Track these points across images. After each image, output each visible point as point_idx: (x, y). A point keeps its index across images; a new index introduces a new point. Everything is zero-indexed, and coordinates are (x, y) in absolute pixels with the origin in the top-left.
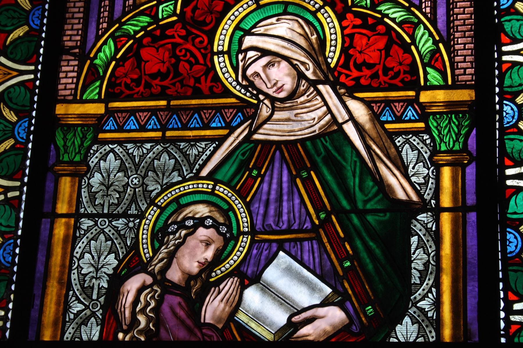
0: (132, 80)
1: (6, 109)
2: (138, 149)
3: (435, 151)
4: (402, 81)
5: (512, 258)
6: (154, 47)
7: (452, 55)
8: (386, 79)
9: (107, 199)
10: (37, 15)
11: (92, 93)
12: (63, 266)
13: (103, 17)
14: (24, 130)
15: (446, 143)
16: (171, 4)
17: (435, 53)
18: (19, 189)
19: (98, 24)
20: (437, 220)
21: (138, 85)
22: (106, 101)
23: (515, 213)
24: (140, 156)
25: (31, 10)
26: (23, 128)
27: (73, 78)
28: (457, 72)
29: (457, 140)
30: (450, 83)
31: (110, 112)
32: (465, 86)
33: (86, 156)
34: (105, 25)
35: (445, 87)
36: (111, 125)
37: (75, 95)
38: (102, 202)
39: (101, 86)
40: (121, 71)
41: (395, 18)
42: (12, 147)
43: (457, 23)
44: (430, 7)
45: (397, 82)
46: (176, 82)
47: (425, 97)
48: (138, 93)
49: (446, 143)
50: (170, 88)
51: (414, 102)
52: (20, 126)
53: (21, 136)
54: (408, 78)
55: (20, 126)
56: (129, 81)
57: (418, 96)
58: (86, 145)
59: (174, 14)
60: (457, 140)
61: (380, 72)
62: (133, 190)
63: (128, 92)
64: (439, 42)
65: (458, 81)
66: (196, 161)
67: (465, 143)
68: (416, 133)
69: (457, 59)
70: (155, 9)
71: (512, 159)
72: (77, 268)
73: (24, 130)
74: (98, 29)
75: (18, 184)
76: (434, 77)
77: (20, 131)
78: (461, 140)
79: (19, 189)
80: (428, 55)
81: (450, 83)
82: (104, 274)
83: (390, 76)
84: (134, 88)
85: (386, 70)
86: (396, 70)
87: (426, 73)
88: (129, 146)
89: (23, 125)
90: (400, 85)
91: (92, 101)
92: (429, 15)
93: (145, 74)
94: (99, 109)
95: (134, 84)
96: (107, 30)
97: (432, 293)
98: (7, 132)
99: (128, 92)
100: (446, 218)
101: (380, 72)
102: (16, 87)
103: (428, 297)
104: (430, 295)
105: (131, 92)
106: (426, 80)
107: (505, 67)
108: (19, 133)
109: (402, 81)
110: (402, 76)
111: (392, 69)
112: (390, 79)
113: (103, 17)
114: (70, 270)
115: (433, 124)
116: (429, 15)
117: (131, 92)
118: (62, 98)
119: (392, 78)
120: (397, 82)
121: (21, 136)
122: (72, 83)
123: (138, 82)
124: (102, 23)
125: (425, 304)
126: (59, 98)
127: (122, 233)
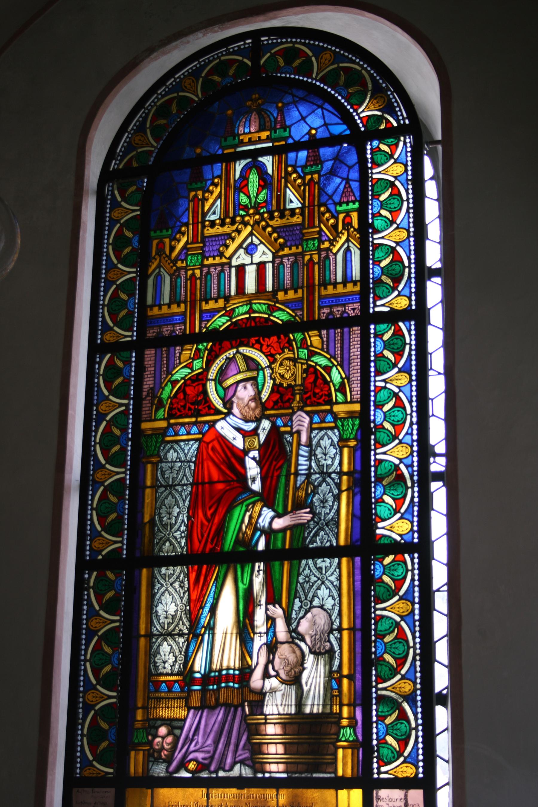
0: (181, 406)
1: (106, 645)
3: (341, 439)
5: (379, 354)
8: (315, 399)
9: (171, 475)
10: (113, 733)
11: (161, 414)
12: (146, 647)
20: (340, 478)
21: (185, 409)
22: (167, 419)
23: (380, 331)
25: (115, 580)
27: (149, 407)
28: (353, 393)
30: (349, 400)
33: (159, 451)
34: (165, 376)
35: (346, 402)
36: (171, 432)
37: (151, 417)
39: (164, 411)
42: (123, 381)
43: (353, 364)
45: (321, 401)
47: (336, 408)
51: (331, 412)
54: (327, 399)
56: (179, 407)
57: (332, 408)
58: (158, 445)
59: (202, 368)
60: (352, 433)
63: (179, 413)
67: (356, 434)
68: (332, 429)
69: (353, 386)
72: (161, 468)
74: (161, 378)
76: (340, 397)
78: (354, 433)
80: (338, 385)
86: (320, 394)
87: (336, 396)
90: (323, 403)
91: (161, 420)
99: (179, 413)
106: (336, 399)
107: (374, 181)
109: (324, 400)
110: (323, 398)
115: (339, 423)
119: (319, 399)
120: (321, 401)
123: (184, 407)
127: (178, 590)
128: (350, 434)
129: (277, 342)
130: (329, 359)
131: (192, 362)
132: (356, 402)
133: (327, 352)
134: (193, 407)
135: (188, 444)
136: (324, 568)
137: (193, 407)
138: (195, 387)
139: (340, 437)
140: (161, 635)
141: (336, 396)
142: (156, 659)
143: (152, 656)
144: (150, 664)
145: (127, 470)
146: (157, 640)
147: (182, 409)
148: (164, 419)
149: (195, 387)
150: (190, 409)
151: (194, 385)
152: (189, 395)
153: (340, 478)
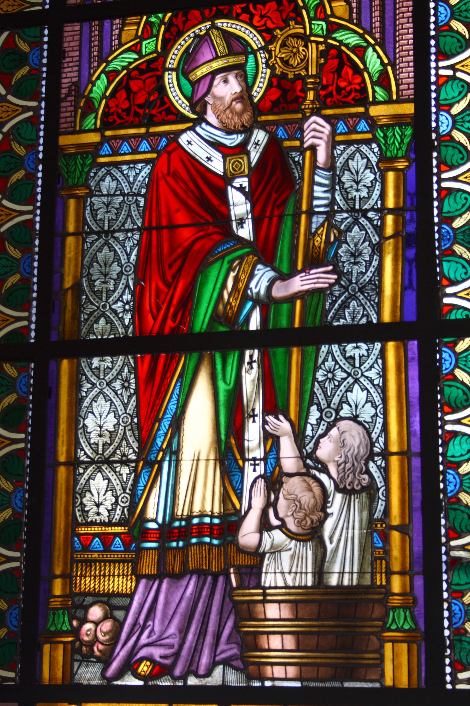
0: (123, 110)
2: (129, 240)
4: (354, 99)
6: (141, 79)
7: (398, 72)
8: (339, 97)
9: (107, 215)
11: (90, 122)
13: (94, 56)
14: (37, 57)
15: (391, 151)
16: (153, 41)
17: (384, 75)
18: (32, 212)
19: (90, 63)
20: (382, 219)
21: (128, 115)
24: (127, 474)
26: (36, 55)
29: (401, 148)
30: (395, 97)
31: (105, 139)
32: (407, 101)
33: (87, 179)
34: (96, 64)
35: (389, 101)
36: (106, 149)
38: (103, 218)
39: (96, 118)
40: (111, 104)
41: (349, 43)
44: (380, 32)
46: (162, 111)
47: (374, 111)
48: (128, 121)
49: (391, 151)
50: (157, 116)
51: (366, 116)
52: (34, 54)
53: (35, 62)
55: (34, 54)
56: (120, 111)
57: (367, 110)
61: (334, 93)
62: (122, 509)
64: (387, 64)
65: (402, 96)
66: (179, 384)
69: (402, 75)
70: (139, 46)
71: (449, 279)
73: (37, 57)
75: (30, 208)
76: (380, 94)
77: (34, 58)
79: (32, 212)
80: (377, 75)
81: (395, 97)
82: (106, 432)
83: (342, 96)
84: (125, 117)
85: (339, 90)
87: (374, 91)
88: (124, 167)
89: (36, 53)
90: (353, 102)
91: (90, 131)
92: (379, 40)
93: (134, 105)
94: (94, 138)
95: (124, 113)
96: (99, 66)
97: (377, 363)
98: (10, 387)
100: (395, 461)
101: (334, 93)
102: (24, 124)
103: (374, 367)
104: (376, 366)
105: (123, 121)
106: (374, 97)
108: (33, 60)
111: (344, 88)
112: (343, 97)
113: (94, 35)
114: (74, 507)
115: (380, 134)
116: (379, 40)
117: (123, 121)
118: (64, 130)
119: (345, 97)
121: (35, 62)
122: (71, 117)
123: (128, 111)
124: (94, 41)
125: (372, 374)
126: (61, 130)
127: (119, 392)
131: (140, 43)
134: (141, 111)
136: (357, 358)
137: (141, 111)
139: (381, 154)
140: (93, 462)
141: (374, 91)
143: (78, 496)
145: (36, 208)
146: (85, 469)
147: (124, 115)
150: (137, 114)
151: (143, 77)
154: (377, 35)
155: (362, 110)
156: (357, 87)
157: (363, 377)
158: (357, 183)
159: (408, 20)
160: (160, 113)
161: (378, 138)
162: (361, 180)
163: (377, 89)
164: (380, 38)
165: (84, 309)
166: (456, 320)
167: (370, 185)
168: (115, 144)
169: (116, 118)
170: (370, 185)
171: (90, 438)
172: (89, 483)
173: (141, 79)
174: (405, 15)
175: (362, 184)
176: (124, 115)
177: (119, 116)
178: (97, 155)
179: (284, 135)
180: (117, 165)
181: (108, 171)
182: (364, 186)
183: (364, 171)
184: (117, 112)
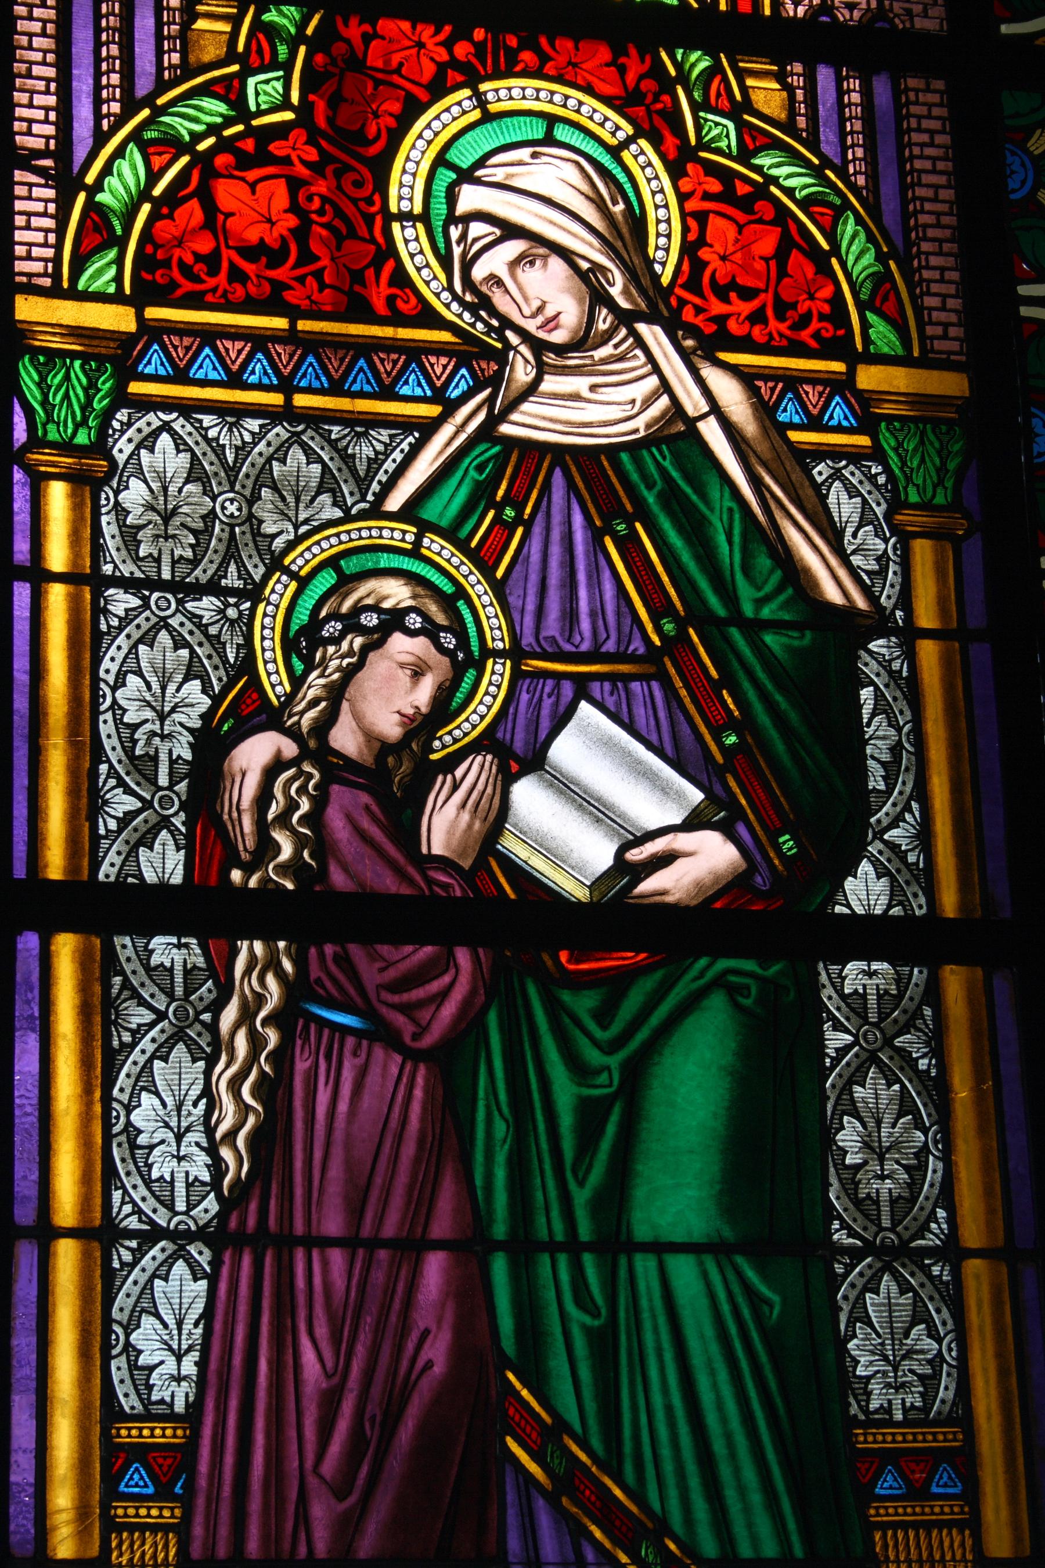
0: (198, 257)
6: (243, 179)
8: (783, 327)
15: (917, 486)
20: (910, 655)
21: (213, 271)
29: (941, 482)
36: (154, 362)
39: (120, 261)
46: (304, 277)
49: (917, 486)
56: (189, 259)
60: (84, 422)
61: (770, 313)
63: (187, 286)
87: (865, 325)
90: (813, 344)
99: (187, 286)
101: (770, 313)
109: (816, 335)
110: (815, 325)
115: (888, 442)
116: (864, 192)
123: (212, 261)
128: (77, 426)
129: (613, 63)
130: (817, 172)
131: (242, 77)
132: (21, 213)
133: (813, 145)
134: (249, 268)
135: (366, 434)
136: (872, 1000)
137: (249, 268)
138: (253, 186)
139: (895, 491)
140: (153, 1234)
141: (865, 325)
142: (133, 1336)
143: (116, 1328)
144: (107, 1359)
146: (138, 1254)
147: (200, 268)
148: (118, 298)
149: (253, 186)
150: (237, 275)
151: (252, 175)
152: (228, 215)
153: (910, 655)
154: (861, 181)
155: (838, 367)
156: (826, 308)
157: (887, 1049)
158: (167, 517)
159: (44, 28)
160: (301, 280)
161: (884, 451)
162: (176, 508)
163: (871, 317)
164: (866, 187)
165: (106, 803)
166: (422, 942)
167: (200, 525)
168: (385, 365)
169: (176, 274)
170: (200, 525)
171: (150, 1167)
172: (152, 1289)
173: (243, 179)
174: (925, 138)
175: (177, 521)
176: (200, 268)
177: (186, 270)
178: (126, 372)
179: (846, 418)
180: (187, 409)
181: (294, 434)
182: (183, 525)
183: (858, 529)
184: (180, 260)
